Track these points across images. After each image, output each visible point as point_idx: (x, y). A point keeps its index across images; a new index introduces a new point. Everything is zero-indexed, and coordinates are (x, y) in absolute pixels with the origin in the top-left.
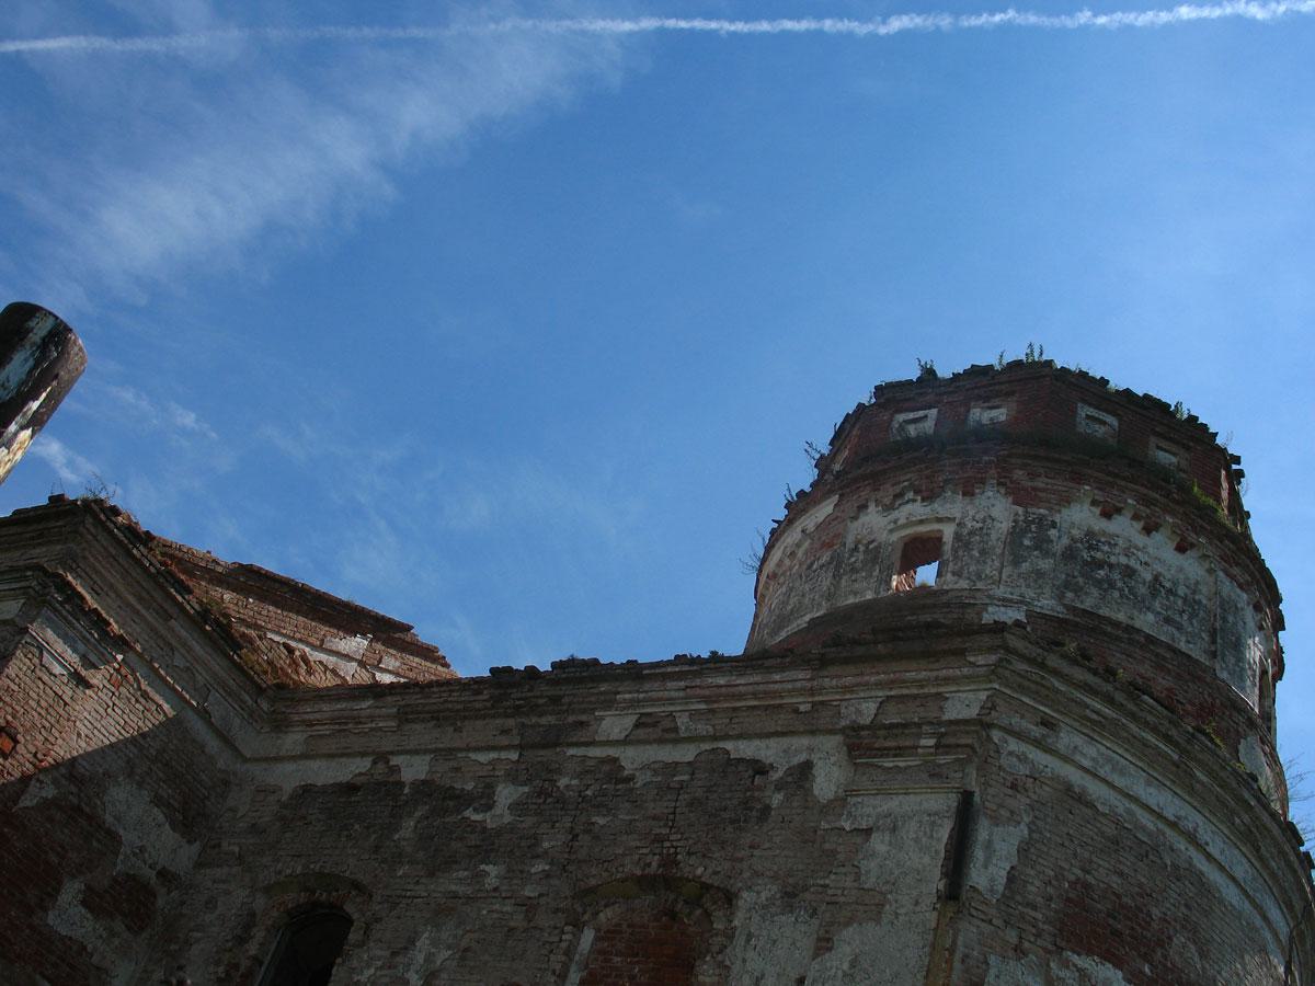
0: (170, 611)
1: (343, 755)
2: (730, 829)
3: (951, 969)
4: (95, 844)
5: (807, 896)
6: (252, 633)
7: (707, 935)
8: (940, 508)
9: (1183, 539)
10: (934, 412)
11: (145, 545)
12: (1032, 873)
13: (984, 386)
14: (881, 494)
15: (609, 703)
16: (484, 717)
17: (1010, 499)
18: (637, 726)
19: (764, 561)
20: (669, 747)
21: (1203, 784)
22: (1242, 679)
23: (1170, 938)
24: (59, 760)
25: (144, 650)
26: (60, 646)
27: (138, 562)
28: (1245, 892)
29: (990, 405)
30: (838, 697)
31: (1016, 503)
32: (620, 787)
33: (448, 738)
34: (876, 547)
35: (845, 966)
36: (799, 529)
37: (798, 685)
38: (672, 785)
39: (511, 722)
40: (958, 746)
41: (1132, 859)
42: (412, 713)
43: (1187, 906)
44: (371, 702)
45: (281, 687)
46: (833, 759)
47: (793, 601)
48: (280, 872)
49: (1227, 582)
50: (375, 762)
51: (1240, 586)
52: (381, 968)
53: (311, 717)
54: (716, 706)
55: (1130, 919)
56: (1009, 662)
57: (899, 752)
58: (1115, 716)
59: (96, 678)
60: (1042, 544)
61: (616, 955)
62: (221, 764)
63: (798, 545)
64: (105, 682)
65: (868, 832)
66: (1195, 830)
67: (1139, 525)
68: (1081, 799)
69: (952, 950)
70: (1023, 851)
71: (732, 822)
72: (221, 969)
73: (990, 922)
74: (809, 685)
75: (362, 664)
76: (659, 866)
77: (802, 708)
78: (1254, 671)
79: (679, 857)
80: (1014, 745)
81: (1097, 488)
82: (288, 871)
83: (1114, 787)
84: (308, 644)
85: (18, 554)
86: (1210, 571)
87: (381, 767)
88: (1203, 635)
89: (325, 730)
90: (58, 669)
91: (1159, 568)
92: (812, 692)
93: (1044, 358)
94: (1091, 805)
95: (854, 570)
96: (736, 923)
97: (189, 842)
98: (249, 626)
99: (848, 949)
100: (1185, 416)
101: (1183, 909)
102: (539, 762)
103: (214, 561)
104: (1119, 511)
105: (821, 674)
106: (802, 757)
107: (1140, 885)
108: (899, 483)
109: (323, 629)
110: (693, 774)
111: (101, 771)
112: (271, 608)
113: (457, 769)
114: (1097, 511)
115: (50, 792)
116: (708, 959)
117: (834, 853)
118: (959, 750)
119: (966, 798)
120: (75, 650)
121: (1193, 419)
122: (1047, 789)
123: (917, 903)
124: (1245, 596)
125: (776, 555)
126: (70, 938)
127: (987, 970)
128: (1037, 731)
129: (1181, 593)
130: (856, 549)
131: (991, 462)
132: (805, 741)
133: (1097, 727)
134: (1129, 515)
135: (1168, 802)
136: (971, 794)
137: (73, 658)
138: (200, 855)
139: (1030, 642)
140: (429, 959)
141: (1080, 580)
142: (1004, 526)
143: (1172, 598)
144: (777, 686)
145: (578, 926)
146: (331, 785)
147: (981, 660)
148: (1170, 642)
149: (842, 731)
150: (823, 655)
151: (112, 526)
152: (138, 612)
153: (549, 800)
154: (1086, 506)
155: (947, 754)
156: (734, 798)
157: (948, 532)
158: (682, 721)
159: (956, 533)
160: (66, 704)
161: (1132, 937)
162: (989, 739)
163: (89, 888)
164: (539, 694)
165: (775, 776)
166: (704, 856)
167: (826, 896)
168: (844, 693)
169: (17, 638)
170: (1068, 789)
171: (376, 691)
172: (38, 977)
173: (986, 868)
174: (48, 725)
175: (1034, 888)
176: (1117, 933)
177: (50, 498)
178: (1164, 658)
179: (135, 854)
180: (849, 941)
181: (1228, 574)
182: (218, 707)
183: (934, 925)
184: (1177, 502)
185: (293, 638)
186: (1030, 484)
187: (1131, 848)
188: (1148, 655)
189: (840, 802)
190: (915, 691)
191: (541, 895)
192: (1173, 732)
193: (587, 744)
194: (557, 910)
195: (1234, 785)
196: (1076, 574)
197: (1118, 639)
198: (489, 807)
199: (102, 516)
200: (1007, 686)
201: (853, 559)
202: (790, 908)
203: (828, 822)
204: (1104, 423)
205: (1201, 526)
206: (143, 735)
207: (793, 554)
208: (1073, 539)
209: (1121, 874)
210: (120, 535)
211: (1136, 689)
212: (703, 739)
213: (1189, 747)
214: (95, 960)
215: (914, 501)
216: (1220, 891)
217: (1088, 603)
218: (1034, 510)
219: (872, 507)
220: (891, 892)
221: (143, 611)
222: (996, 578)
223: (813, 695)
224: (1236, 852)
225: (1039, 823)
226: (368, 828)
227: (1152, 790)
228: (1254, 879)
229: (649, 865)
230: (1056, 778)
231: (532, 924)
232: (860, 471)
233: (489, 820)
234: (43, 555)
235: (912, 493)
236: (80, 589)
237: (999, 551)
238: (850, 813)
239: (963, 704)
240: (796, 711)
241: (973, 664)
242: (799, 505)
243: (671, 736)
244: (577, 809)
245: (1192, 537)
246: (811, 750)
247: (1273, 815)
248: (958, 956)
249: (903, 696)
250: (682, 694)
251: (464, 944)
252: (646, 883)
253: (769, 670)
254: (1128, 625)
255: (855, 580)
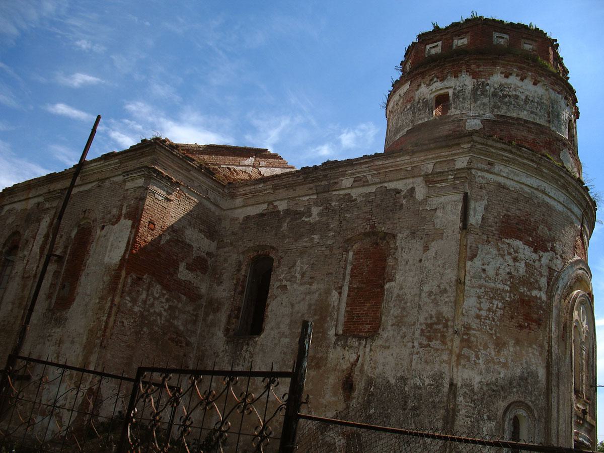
0: (190, 168)
1: (257, 204)
2: (391, 213)
3: (466, 251)
4: (185, 250)
5: (419, 233)
6: (216, 167)
7: (389, 249)
8: (446, 83)
9: (536, 80)
10: (440, 42)
11: (177, 149)
12: (490, 215)
13: (458, 30)
14: (425, 80)
15: (344, 175)
16: (303, 184)
17: (471, 77)
18: (354, 181)
19: (387, 105)
20: (366, 188)
21: (546, 173)
22: (560, 128)
23: (538, 227)
24: (168, 226)
25: (184, 184)
26: (159, 191)
27: (176, 156)
28: (564, 206)
29: (460, 37)
30: (420, 164)
31: (473, 78)
32: (352, 203)
33: (292, 194)
34: (426, 101)
35: (434, 255)
36: (398, 94)
37: (406, 161)
38: (370, 201)
39: (312, 185)
40: (461, 177)
41: (523, 204)
42: (277, 186)
43: (543, 215)
44: (262, 185)
45: (230, 183)
46: (421, 185)
47: (400, 123)
48: (246, 247)
49: (553, 93)
50: (268, 205)
51: (558, 93)
52: (286, 274)
53: (243, 192)
54: (379, 171)
55: (524, 224)
56: (475, 146)
57: (442, 181)
58: (513, 157)
59: (172, 197)
60: (484, 93)
61: (361, 259)
62: (217, 214)
63: (399, 101)
64: (175, 198)
65: (435, 209)
66: (545, 189)
67: (519, 78)
68: (504, 187)
69: (466, 245)
70: (486, 209)
71: (391, 211)
72: (235, 281)
73: (477, 234)
74: (409, 161)
75: (254, 167)
76: (370, 229)
77: (408, 169)
78: (566, 123)
79: (376, 225)
80: (480, 173)
81: (502, 67)
82: (249, 246)
83: (515, 181)
84: (235, 165)
85: (136, 161)
86: (547, 90)
87: (271, 206)
88: (545, 115)
89: (249, 196)
90: (161, 198)
91: (527, 93)
92: (411, 163)
93: (478, 16)
94: (508, 189)
95: (420, 110)
96: (397, 244)
97: (213, 241)
98: (214, 165)
99: (434, 249)
100: (534, 27)
101: (542, 216)
102: (324, 198)
103: (199, 147)
104: (511, 74)
105: (413, 156)
106: (411, 186)
107: (527, 212)
108: (431, 75)
109: (239, 159)
110: (376, 196)
111: (181, 226)
112: (220, 157)
113: (297, 204)
114: (503, 75)
115: (168, 237)
116: (390, 257)
117: (425, 218)
118: (461, 178)
119: (466, 195)
120: (164, 191)
121: (537, 29)
122: (493, 186)
123: (453, 232)
124: (560, 96)
125: (391, 104)
126: (186, 280)
127: (478, 250)
128: (486, 167)
129: (536, 101)
130: (419, 102)
131: (462, 63)
132: (411, 180)
133: (507, 162)
134: (515, 75)
135: (534, 182)
136: (467, 193)
137: (164, 193)
138: (217, 245)
139: (481, 137)
140: (302, 269)
141: (499, 104)
142: (470, 87)
143: (533, 104)
144: (399, 163)
145: (347, 251)
146: (256, 215)
147: (465, 146)
148: (533, 121)
149: (423, 176)
150: (413, 150)
151: (165, 146)
152: (179, 172)
153: (330, 211)
154: (499, 74)
155: (458, 180)
156: (390, 202)
157: (451, 92)
158: (369, 178)
159: (453, 92)
160: (166, 208)
161: (525, 229)
162: (471, 173)
163: (187, 264)
164: (319, 175)
165: (403, 193)
166: (384, 223)
167: (425, 233)
168: (421, 162)
169: (146, 192)
170: (499, 185)
171: (264, 180)
172: (180, 294)
173: (474, 217)
174: (162, 217)
175: (491, 220)
176: (519, 229)
177: (141, 141)
178: (531, 128)
179: (198, 250)
180: (434, 246)
181: (553, 90)
182: (212, 195)
183: (459, 238)
184: (532, 67)
185: (230, 165)
186: (478, 70)
187: (523, 200)
188: (525, 128)
189: (425, 200)
190: (445, 159)
191: (333, 243)
192: (534, 158)
193: (338, 190)
194: (340, 247)
195: (557, 171)
196: (497, 101)
197: (514, 124)
198: (310, 216)
199: (161, 144)
200: (475, 154)
201: (419, 106)
202: (414, 238)
203: (422, 208)
204: (503, 38)
205: (542, 73)
206: (191, 211)
207: (397, 104)
208: (495, 89)
209: (520, 210)
210: (168, 149)
211: (520, 146)
212: (376, 184)
213: (540, 162)
214: (195, 285)
215: (437, 81)
216: (554, 207)
217: (502, 112)
218: (480, 80)
219: (423, 85)
220: (445, 229)
221: (181, 171)
222: (469, 108)
223: (411, 164)
224: (560, 193)
225: (491, 198)
226: (271, 228)
227: (529, 179)
228: (567, 200)
229: (367, 229)
230: (495, 182)
231: (333, 253)
232: (416, 72)
233: (311, 220)
234: (146, 161)
235: (436, 79)
236: (160, 170)
237: (469, 97)
238: (429, 204)
239: (461, 162)
240: (407, 170)
241: (463, 148)
242: (397, 85)
243: (366, 184)
244: (339, 213)
245: (539, 79)
246: (413, 183)
247: (573, 178)
248: (468, 247)
249: (441, 161)
250: (367, 169)
251: (312, 262)
252: (367, 235)
253: (396, 157)
254: (517, 118)
255: (421, 114)
